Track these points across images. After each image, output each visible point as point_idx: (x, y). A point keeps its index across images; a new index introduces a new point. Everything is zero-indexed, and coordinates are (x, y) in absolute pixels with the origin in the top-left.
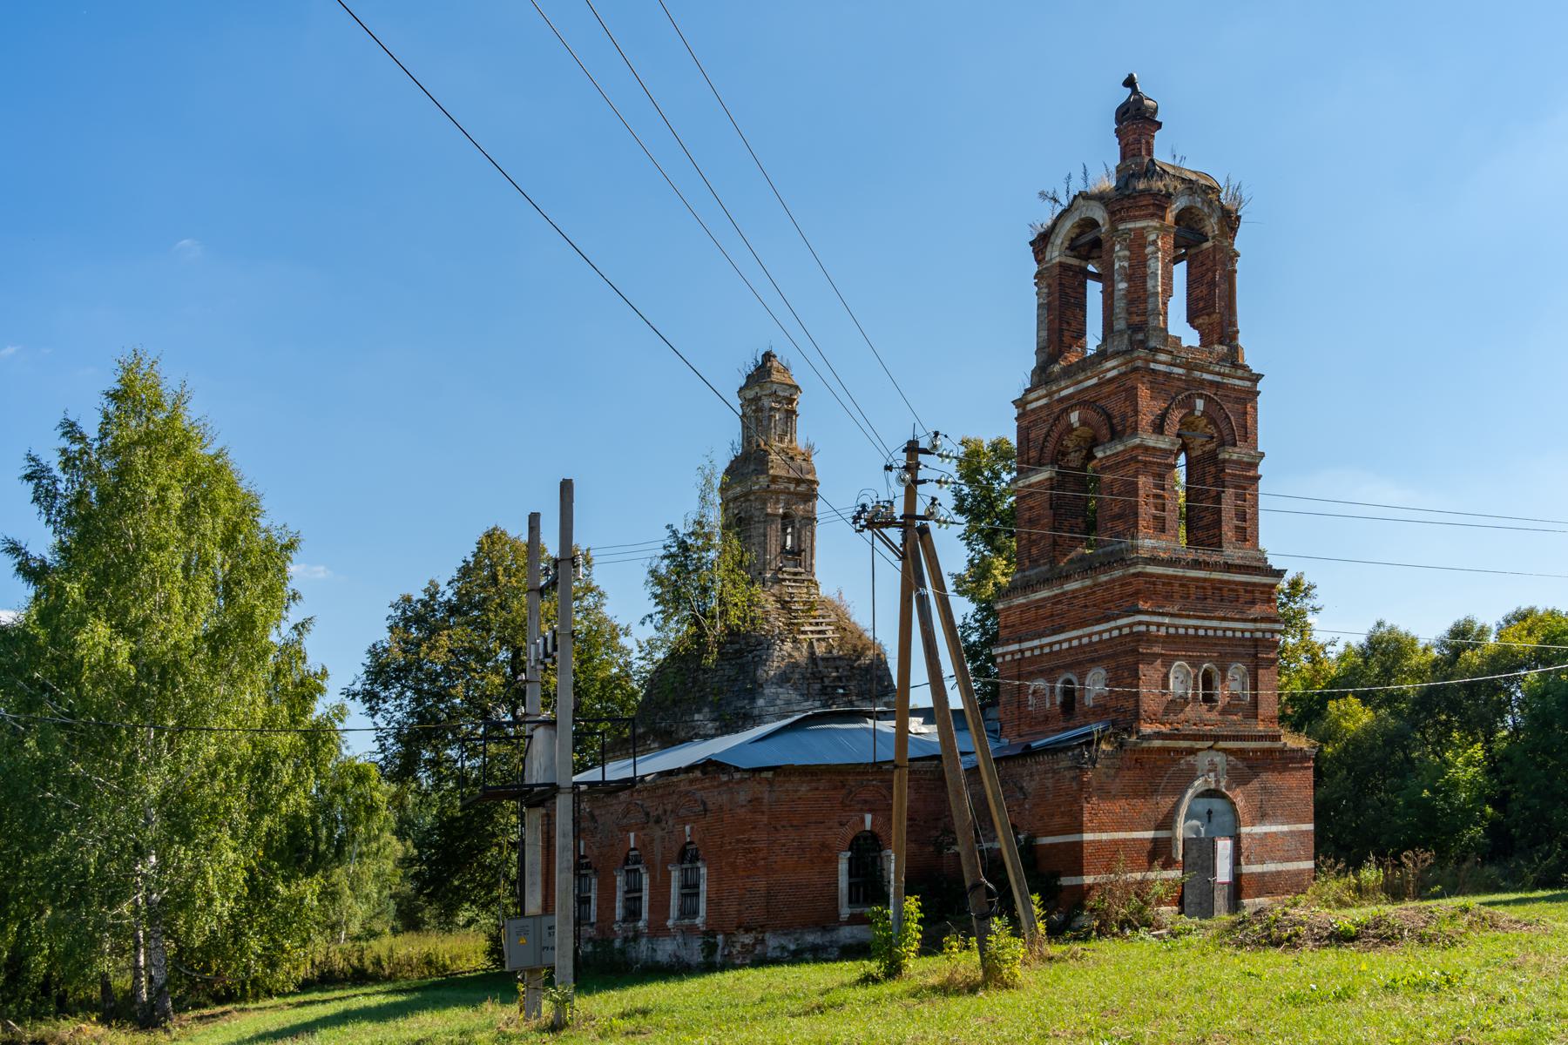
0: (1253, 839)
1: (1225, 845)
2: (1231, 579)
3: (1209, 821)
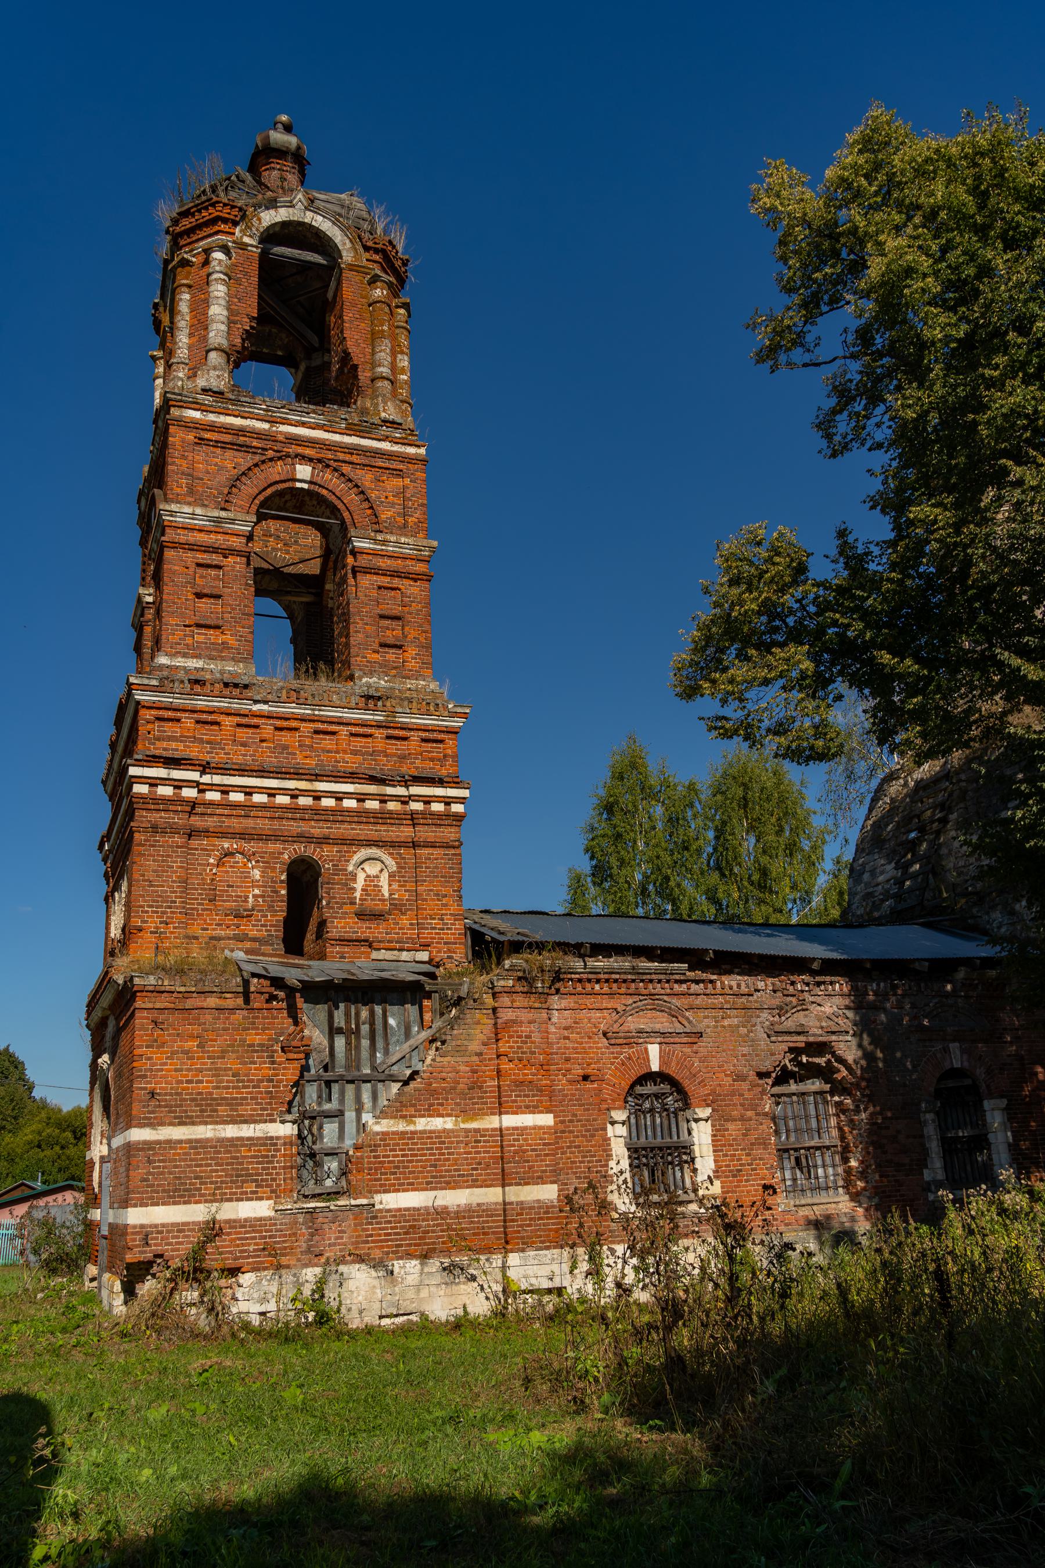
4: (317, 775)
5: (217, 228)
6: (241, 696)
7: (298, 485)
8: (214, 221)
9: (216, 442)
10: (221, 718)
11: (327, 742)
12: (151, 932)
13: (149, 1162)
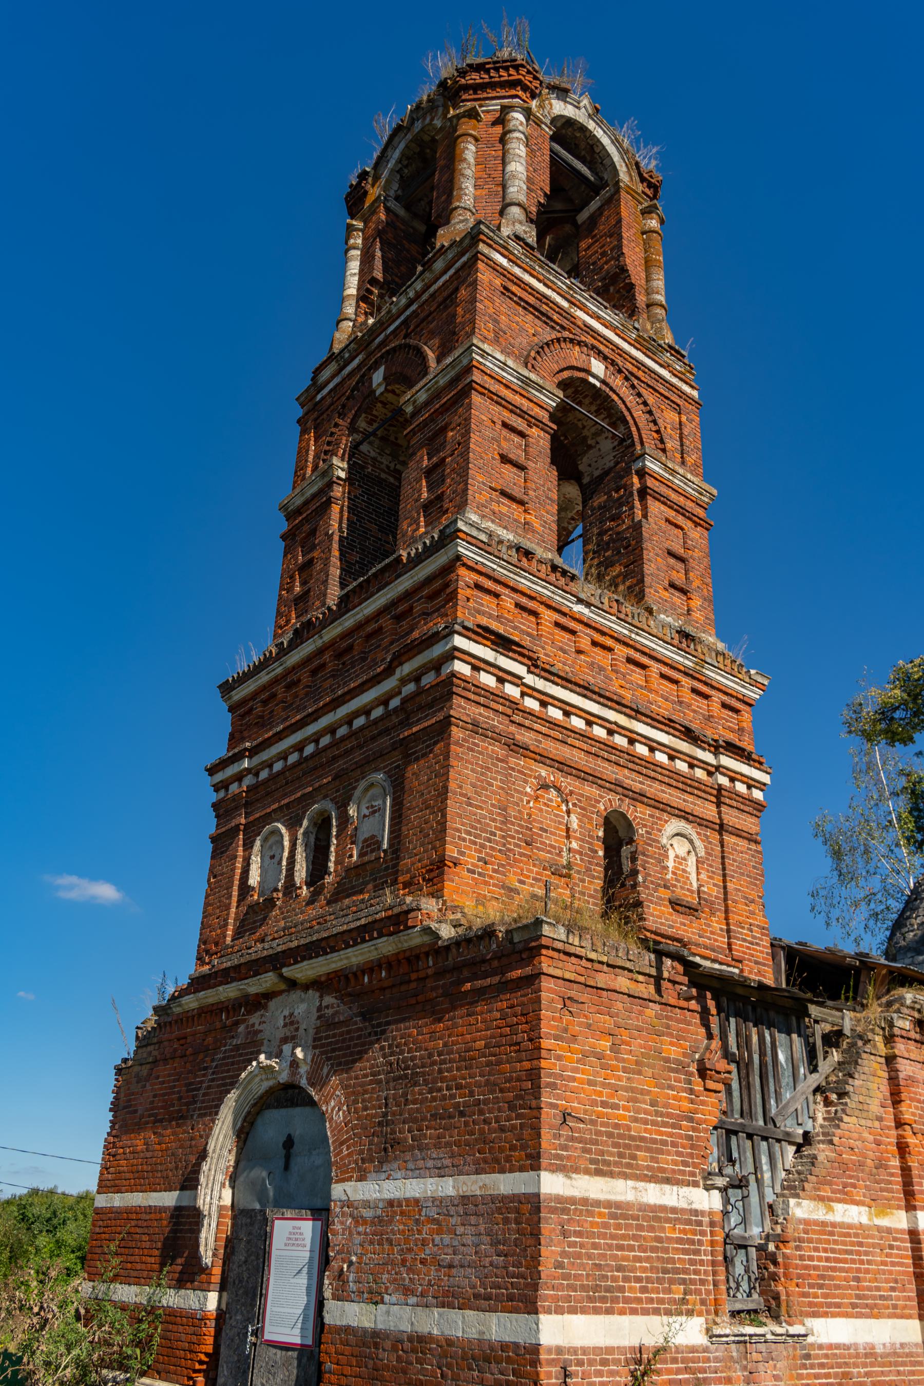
0: (358, 1220)
1: (296, 1232)
2: (360, 617)
3: (287, 1167)
4: (637, 712)
5: (513, 92)
6: (565, 588)
7: (591, 380)
8: (513, 84)
9: (520, 298)
10: (541, 609)
11: (637, 676)
12: (469, 871)
13: (565, 1234)
